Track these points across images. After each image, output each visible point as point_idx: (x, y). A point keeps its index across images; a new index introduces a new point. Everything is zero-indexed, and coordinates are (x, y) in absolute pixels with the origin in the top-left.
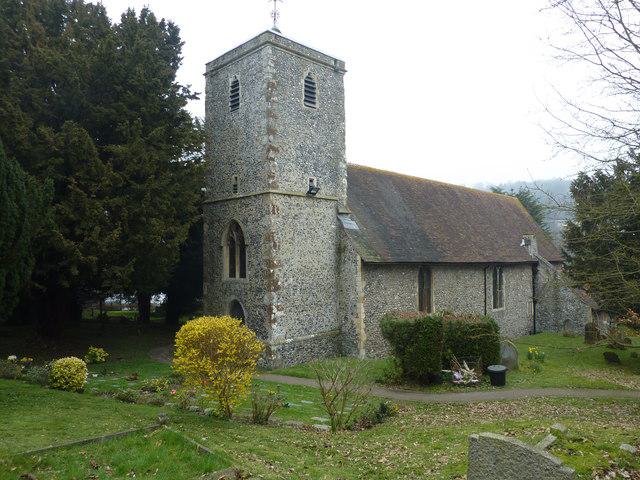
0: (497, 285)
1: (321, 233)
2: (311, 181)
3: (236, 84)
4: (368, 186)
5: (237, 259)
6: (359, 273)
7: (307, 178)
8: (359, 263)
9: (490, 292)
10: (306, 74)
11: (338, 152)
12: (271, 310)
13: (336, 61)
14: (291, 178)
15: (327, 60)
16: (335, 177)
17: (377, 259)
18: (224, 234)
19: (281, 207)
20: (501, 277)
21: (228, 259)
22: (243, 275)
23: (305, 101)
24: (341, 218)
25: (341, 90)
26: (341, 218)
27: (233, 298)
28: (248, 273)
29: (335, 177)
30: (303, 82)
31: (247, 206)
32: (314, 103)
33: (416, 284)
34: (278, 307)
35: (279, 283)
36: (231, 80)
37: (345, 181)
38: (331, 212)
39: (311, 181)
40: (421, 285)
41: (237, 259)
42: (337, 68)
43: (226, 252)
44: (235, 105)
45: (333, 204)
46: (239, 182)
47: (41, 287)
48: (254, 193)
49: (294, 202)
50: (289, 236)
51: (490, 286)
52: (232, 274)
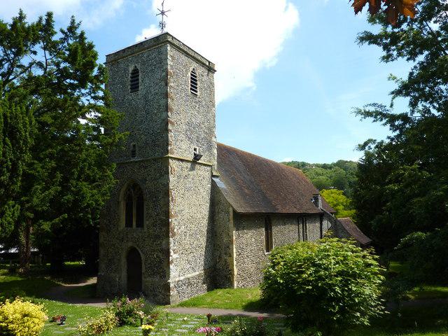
0: (305, 229)
1: (202, 190)
2: (195, 150)
3: (135, 72)
4: (227, 155)
5: (134, 212)
6: (232, 221)
7: (193, 147)
8: (231, 214)
9: (301, 234)
10: (191, 69)
11: (211, 131)
12: (168, 253)
13: (209, 62)
14: (180, 146)
15: (204, 61)
16: (210, 148)
17: (250, 210)
18: (122, 193)
19: (176, 169)
20: (306, 226)
21: (124, 217)
22: (140, 224)
23: (191, 89)
24: (214, 179)
25: (212, 84)
26: (214, 179)
27: (130, 244)
28: (146, 223)
29: (210, 148)
30: (190, 74)
31: (146, 168)
32: (196, 92)
33: (264, 229)
34: (174, 250)
35: (175, 230)
36: (131, 69)
37: (215, 151)
38: (208, 175)
39: (195, 150)
40: (266, 230)
41: (134, 212)
42: (210, 69)
43: (123, 206)
44: (135, 87)
45: (209, 168)
46: (137, 149)
47: (72, 81)
48: (153, 157)
49: (185, 165)
50: (182, 192)
51: (301, 230)
52: (129, 224)
